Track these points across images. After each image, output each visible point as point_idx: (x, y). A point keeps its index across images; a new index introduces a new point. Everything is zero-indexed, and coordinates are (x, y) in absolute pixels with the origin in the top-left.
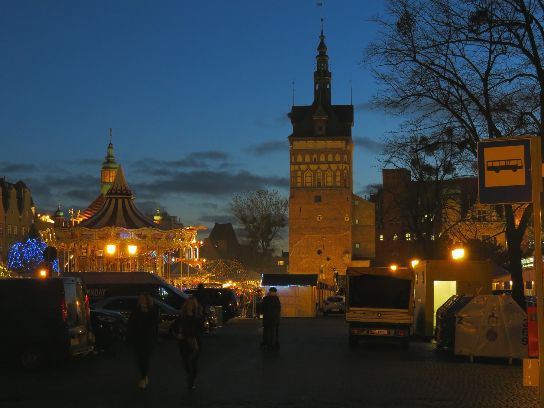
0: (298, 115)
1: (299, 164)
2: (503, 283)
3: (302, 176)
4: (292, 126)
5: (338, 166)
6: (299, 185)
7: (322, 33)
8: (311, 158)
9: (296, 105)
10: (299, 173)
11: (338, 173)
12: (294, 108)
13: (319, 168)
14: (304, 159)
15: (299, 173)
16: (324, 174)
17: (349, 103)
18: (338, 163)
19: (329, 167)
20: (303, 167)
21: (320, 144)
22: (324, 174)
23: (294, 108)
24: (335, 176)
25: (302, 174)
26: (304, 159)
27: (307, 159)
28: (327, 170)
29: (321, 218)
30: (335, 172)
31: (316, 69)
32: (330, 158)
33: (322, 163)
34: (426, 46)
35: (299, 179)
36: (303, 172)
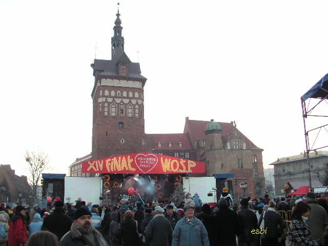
0: (99, 68)
1: (106, 97)
2: (245, 148)
3: (109, 107)
4: (125, 51)
5: (137, 102)
6: (106, 114)
7: (118, 12)
8: (116, 93)
9: (97, 58)
10: (106, 105)
11: (137, 107)
12: (96, 60)
13: (122, 101)
14: (110, 93)
15: (106, 105)
16: (126, 107)
17: (137, 62)
18: (136, 99)
19: (130, 102)
20: (110, 100)
21: (123, 83)
22: (126, 107)
23: (96, 60)
24: (135, 109)
25: (109, 105)
26: (110, 93)
27: (125, 94)
28: (128, 103)
29: (124, 141)
30: (134, 106)
31: (113, 36)
32: (131, 95)
33: (124, 98)
34: (282, 173)
35: (106, 109)
36: (109, 103)
